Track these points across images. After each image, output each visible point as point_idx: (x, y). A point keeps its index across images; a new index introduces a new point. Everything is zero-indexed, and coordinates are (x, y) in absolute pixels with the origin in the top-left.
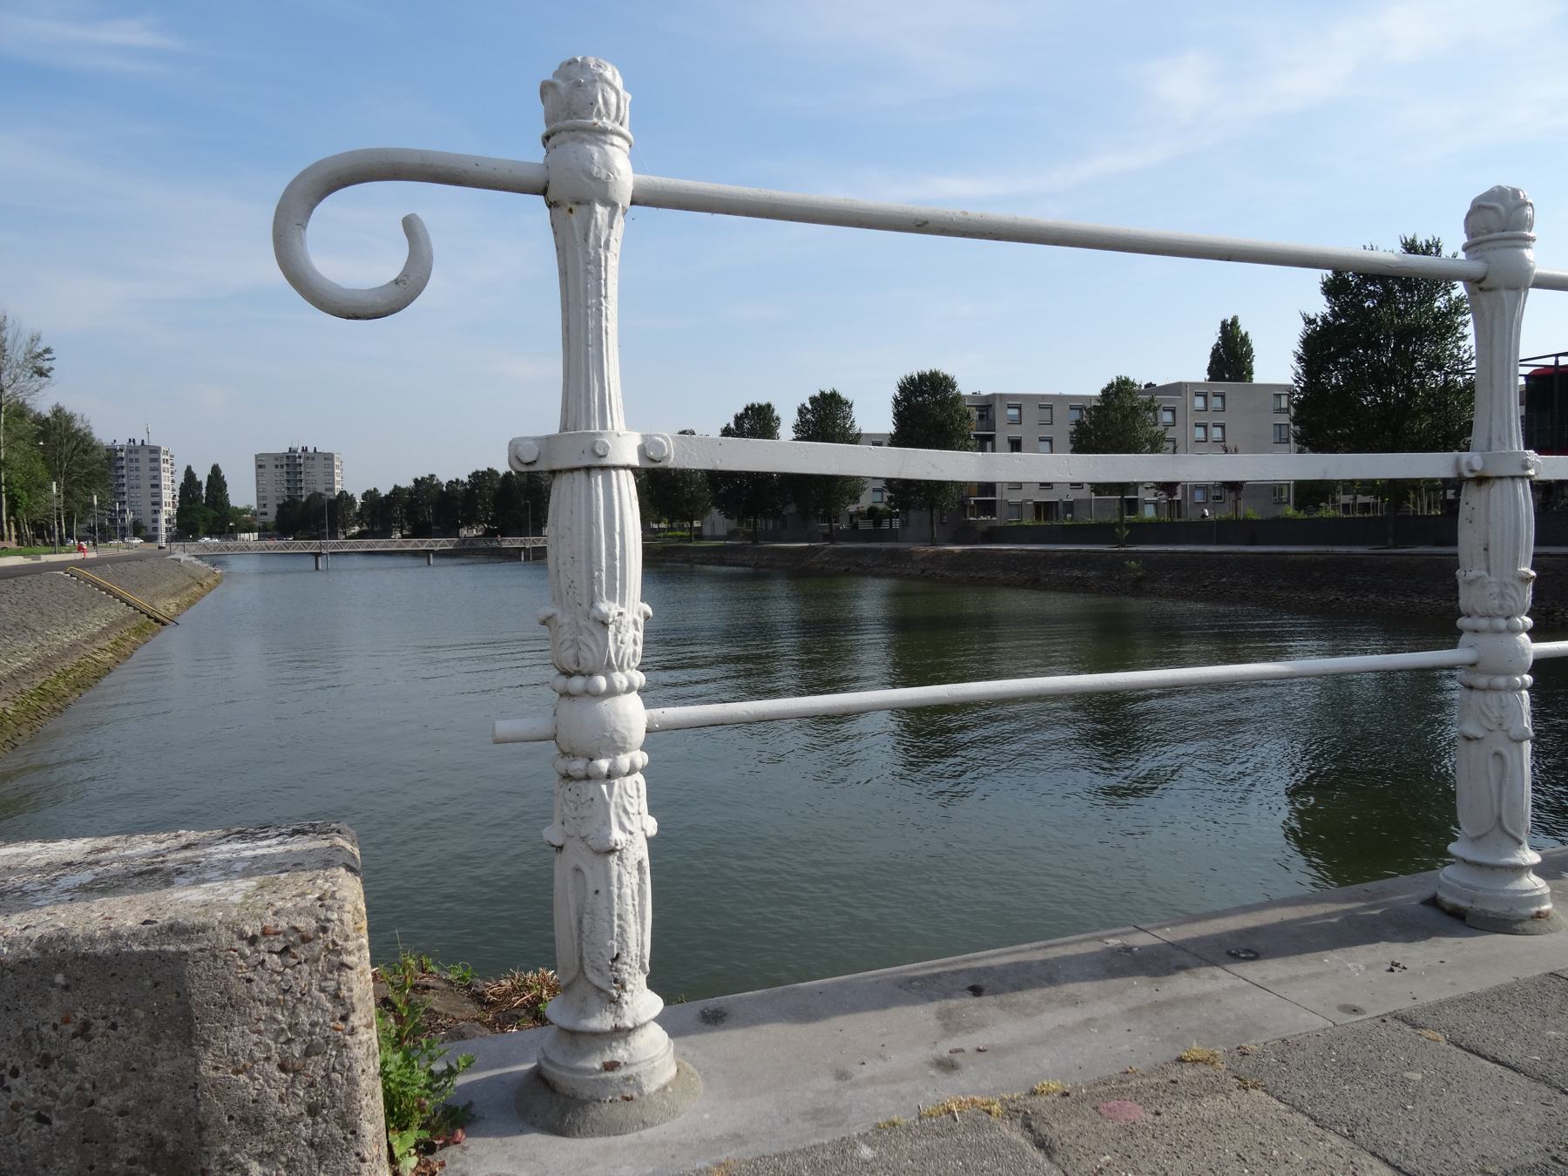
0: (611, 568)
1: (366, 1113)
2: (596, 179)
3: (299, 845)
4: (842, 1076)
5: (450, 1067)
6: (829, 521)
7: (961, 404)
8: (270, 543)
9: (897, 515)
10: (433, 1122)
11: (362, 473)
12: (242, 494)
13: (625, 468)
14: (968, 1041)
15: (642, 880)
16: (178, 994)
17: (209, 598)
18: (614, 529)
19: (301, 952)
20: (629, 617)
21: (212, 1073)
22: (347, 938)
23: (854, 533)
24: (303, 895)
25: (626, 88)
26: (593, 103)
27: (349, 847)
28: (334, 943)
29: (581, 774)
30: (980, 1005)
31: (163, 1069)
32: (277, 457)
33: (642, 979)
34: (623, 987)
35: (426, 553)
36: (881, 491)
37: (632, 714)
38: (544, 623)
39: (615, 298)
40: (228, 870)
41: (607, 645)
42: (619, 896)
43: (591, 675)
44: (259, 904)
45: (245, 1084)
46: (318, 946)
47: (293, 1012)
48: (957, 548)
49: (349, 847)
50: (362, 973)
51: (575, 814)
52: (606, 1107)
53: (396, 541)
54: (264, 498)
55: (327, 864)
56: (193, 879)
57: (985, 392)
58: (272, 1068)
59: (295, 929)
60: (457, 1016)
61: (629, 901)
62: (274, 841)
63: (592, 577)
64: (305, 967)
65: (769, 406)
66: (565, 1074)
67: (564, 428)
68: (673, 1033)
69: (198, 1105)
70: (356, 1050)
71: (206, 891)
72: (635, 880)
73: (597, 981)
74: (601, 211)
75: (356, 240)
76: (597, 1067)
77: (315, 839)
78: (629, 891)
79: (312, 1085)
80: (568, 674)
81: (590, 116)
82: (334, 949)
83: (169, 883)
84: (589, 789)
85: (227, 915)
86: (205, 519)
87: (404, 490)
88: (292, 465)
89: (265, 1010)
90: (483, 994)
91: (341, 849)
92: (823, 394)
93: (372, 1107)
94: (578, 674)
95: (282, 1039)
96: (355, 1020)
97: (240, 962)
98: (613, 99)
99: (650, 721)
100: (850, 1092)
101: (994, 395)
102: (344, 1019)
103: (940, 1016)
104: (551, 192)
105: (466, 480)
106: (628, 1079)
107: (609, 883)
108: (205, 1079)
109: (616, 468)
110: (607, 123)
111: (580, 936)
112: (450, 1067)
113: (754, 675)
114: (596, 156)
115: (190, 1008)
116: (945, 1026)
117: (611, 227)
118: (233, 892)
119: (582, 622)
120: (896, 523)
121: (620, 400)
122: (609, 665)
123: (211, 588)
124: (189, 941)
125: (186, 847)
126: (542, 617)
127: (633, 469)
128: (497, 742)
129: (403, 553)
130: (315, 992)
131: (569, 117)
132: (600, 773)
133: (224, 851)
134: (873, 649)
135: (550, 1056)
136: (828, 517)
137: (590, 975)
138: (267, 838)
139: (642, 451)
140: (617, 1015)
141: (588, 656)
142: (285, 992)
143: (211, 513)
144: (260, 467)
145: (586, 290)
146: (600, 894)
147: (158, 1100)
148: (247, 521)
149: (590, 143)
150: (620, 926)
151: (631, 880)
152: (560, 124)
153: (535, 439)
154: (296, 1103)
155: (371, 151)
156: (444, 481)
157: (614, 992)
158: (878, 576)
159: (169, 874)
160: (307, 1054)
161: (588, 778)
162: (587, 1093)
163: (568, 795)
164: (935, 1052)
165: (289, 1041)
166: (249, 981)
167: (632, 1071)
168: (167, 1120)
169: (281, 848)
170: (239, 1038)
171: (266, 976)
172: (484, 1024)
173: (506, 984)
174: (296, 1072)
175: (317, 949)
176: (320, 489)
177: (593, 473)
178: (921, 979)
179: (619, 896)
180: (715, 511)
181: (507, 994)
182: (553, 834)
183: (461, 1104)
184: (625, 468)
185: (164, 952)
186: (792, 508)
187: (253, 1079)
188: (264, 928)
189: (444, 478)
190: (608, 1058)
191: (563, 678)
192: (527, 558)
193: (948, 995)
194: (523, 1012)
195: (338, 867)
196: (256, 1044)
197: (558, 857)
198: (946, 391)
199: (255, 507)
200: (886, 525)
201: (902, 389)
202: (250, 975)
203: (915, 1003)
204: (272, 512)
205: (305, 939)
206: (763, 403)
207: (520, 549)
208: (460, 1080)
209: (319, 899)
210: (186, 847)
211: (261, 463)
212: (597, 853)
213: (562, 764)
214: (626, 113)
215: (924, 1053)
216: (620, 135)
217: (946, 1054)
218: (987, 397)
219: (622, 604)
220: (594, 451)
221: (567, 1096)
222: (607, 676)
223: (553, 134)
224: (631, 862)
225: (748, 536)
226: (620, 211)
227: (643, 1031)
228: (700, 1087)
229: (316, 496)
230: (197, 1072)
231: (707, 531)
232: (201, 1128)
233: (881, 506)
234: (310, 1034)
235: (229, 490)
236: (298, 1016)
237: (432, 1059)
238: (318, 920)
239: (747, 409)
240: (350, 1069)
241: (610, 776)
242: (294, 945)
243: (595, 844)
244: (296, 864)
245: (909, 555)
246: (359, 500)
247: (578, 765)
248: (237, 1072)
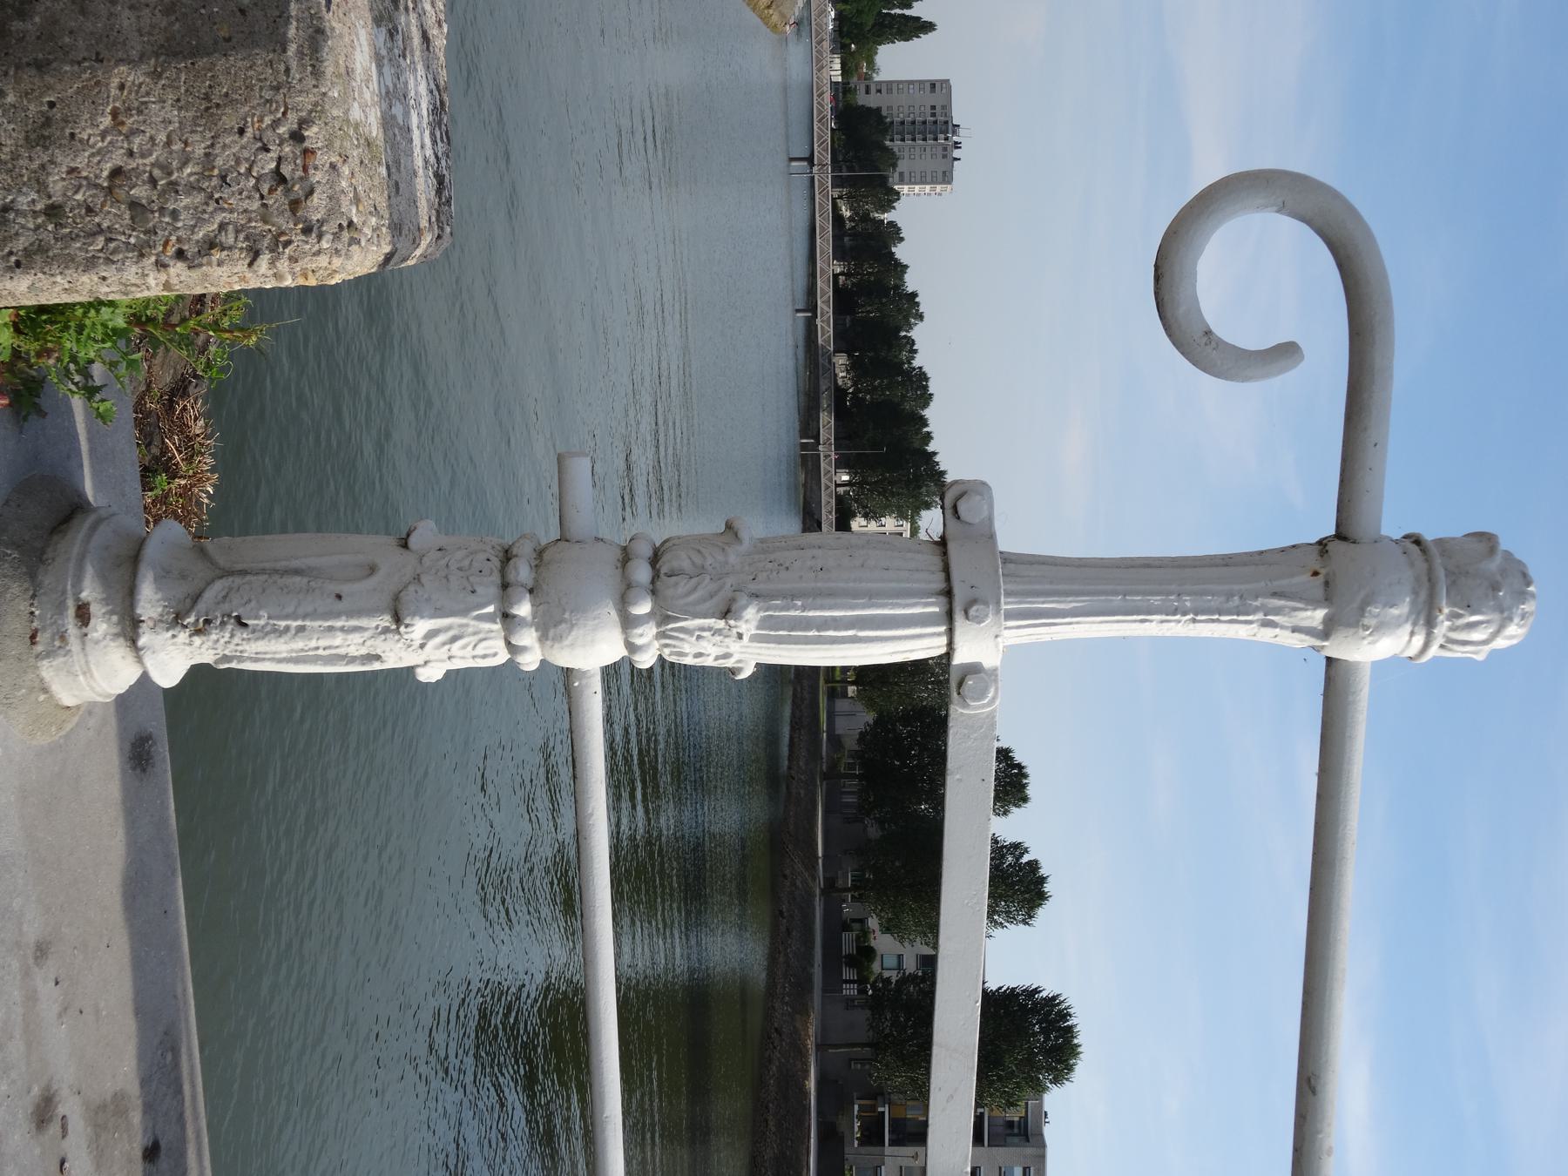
0: (807, 624)
1: (43, 280)
2: (1362, 611)
3: (424, 186)
4: (42, 951)
5: (98, 389)
6: (855, 888)
7: (1029, 1092)
8: (827, 96)
9: (862, 991)
10: (21, 365)
11: (923, 221)
12: (895, 62)
13: (950, 644)
14: (77, 1147)
15: (353, 660)
16: (228, 40)
17: (754, 19)
18: (862, 628)
19: (278, 200)
20: (734, 647)
21: (115, 82)
22: (293, 260)
23: (837, 925)
24: (357, 200)
25: (1494, 651)
26: (1470, 608)
27: (418, 252)
28: (288, 243)
29: (511, 577)
30: (130, 1161)
31: (126, 19)
32: (947, 107)
33: (207, 657)
34: (198, 632)
35: (812, 307)
36: (899, 967)
37: (594, 649)
38: (729, 526)
39: (1192, 634)
40: (394, 95)
41: (696, 616)
42: (331, 629)
43: (654, 592)
44: (347, 144)
45: (94, 127)
46: (284, 222)
47: (193, 188)
48: (812, 1084)
49: (418, 252)
50: (243, 279)
51: (453, 567)
52: (24, 607)
53: (830, 267)
54: (890, 91)
55: (396, 228)
56: (384, 52)
57: (1048, 1131)
58: (117, 159)
59: (311, 192)
60: (158, 360)
61: (322, 643)
62: (429, 152)
63: (794, 597)
64: (256, 205)
65: (1025, 799)
66: (76, 550)
67: (1008, 559)
68: (123, 702)
69: (72, 63)
70: (134, 269)
71: (367, 71)
72: (353, 651)
73: (210, 595)
74: (1316, 616)
75: (1263, 277)
76: (84, 595)
77: (431, 207)
78: (337, 642)
79: (90, 210)
80: (655, 559)
81: (1452, 603)
82: (278, 243)
83: (378, 21)
84: (489, 586)
85: (334, 102)
86: (860, 12)
87: (901, 278)
88: (935, 126)
89: (199, 151)
90: (185, 395)
91: (415, 243)
92: (1043, 880)
93: (52, 288)
94: (655, 576)
95: (157, 173)
96: (177, 269)
97: (267, 120)
98: (1476, 636)
99: (582, 674)
100: (15, 965)
101: (1043, 1146)
102: (180, 254)
103: (119, 1097)
104: (1336, 547)
105: (916, 363)
106: (63, 638)
107: (350, 614)
108: (108, 71)
109: (950, 632)
110: (1443, 627)
111: (276, 571)
112: (98, 389)
113: (635, 772)
114: (1395, 611)
115: (208, 54)
116: (103, 1107)
117: (1295, 630)
118: (364, 107)
119: (729, 581)
120: (850, 990)
121: (1047, 638)
122: (667, 619)
123: (765, 20)
124: (300, 54)
125: (425, 38)
126: (736, 525)
127: (948, 655)
128: (560, 459)
129: (812, 275)
130: (219, 218)
131: (1448, 573)
132: (511, 605)
133: (419, 88)
134: (669, 954)
135: (102, 528)
136: (860, 886)
137: (219, 586)
138: (434, 142)
139: (974, 669)
140: (157, 623)
141: (681, 590)
142: (223, 178)
143: (869, 21)
144: (933, 85)
145: (1205, 593)
146: (333, 598)
147: (83, 12)
148: (858, 67)
149: (1413, 603)
150: (287, 629)
151: (353, 645)
152: (1438, 561)
153: (990, 519)
154: (66, 189)
155: (1388, 302)
156: (914, 334)
157: (191, 619)
158: (772, 959)
159: (391, 19)
160: (134, 205)
161: (505, 586)
162: (47, 580)
163: (482, 556)
164: (65, 1092)
165: (153, 182)
166: (241, 132)
167: (74, 644)
168: (55, 22)
169: (419, 162)
170: (163, 116)
171: (246, 154)
172: (142, 397)
173: (198, 427)
174: (110, 191)
175: (280, 221)
176: (903, 166)
177: (943, 600)
178: (176, 1065)
179: (331, 629)
180: (870, 717)
181: (183, 427)
182: (426, 534)
183: (44, 402)
184: (950, 644)
185: (287, 22)
186: (874, 832)
187: (103, 135)
188: (313, 152)
189: (918, 333)
190: (95, 609)
191: (649, 552)
192: (804, 447)
193: (149, 1108)
194: (155, 451)
195: (393, 243)
196: (152, 138)
197: (391, 541)
198: (1050, 1069)
199: (877, 78)
200: (848, 973)
201: (1052, 1001)
202: (249, 132)
203: (141, 1056)
204: (871, 101)
205: (295, 205)
206: (1030, 791)
207: (817, 437)
208: (77, 403)
209: (351, 224)
210: (425, 38)
211: (939, 88)
212: (396, 598)
213: (525, 550)
214: (1459, 652)
215: (65, 1075)
216: (1426, 646)
217: (61, 1110)
218: (1041, 1135)
219: (754, 638)
220: (974, 602)
221: (43, 552)
222: (651, 615)
223: (1424, 551)
224: (379, 646)
225: (833, 765)
226: (1318, 643)
227: (130, 658)
228: (42, 740)
229: (892, 159)
230: (121, 61)
231: (841, 705)
232: (40, 66)
233: (876, 967)
234: (162, 210)
235: (900, 45)
236: (188, 194)
237: (113, 365)
238: (321, 222)
239: (1020, 767)
240: (109, 261)
241: (506, 617)
242: (288, 191)
243: (409, 595)
244: (397, 186)
245: (802, 1009)
246: (887, 217)
247: (522, 572)
248: (115, 114)
